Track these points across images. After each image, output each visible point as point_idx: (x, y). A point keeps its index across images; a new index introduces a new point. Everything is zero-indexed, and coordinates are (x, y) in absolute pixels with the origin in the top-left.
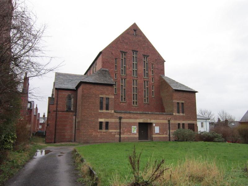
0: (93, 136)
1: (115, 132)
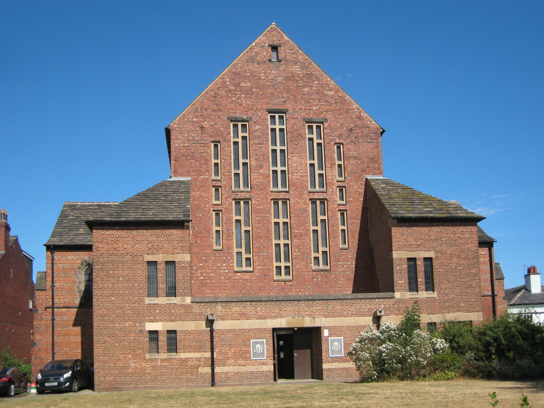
0: (130, 371)
1: (198, 359)
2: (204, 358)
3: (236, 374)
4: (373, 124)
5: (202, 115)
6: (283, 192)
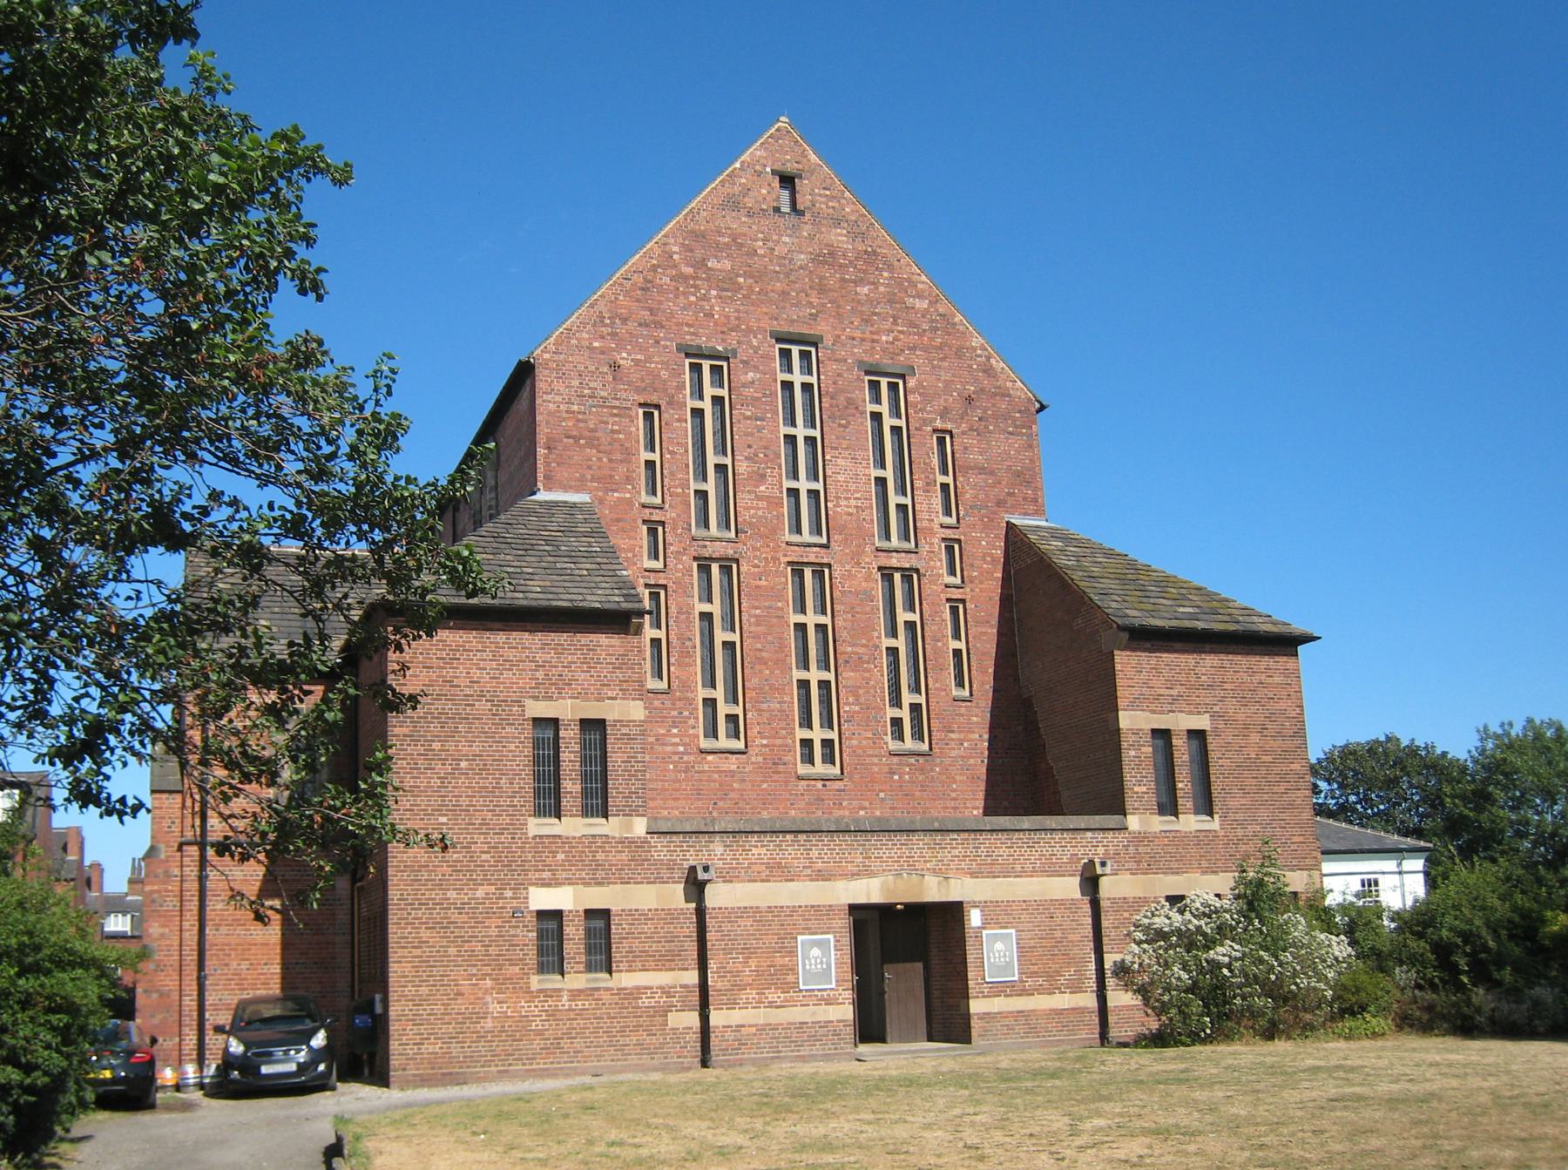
1: (666, 991)
2: (681, 986)
3: (761, 1029)
4: (1019, 390)
5: (614, 335)
6: (815, 545)
